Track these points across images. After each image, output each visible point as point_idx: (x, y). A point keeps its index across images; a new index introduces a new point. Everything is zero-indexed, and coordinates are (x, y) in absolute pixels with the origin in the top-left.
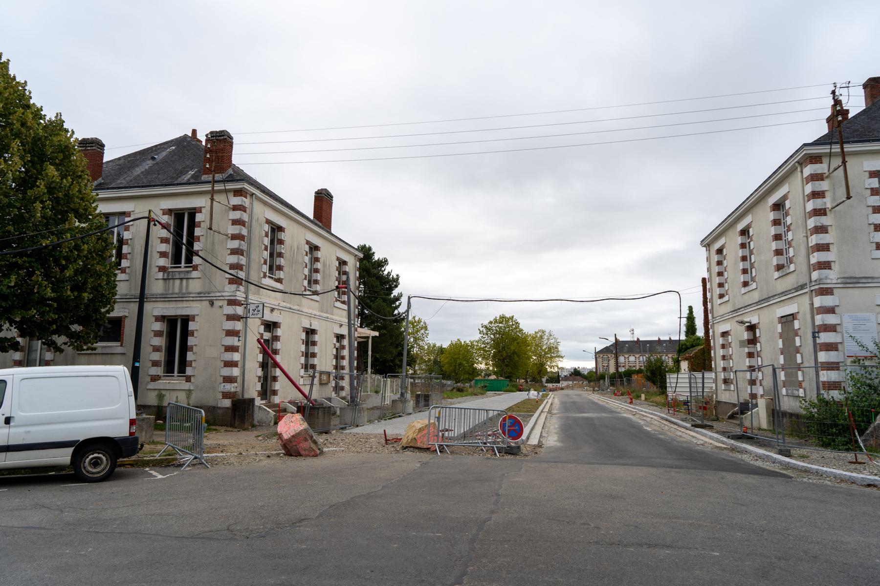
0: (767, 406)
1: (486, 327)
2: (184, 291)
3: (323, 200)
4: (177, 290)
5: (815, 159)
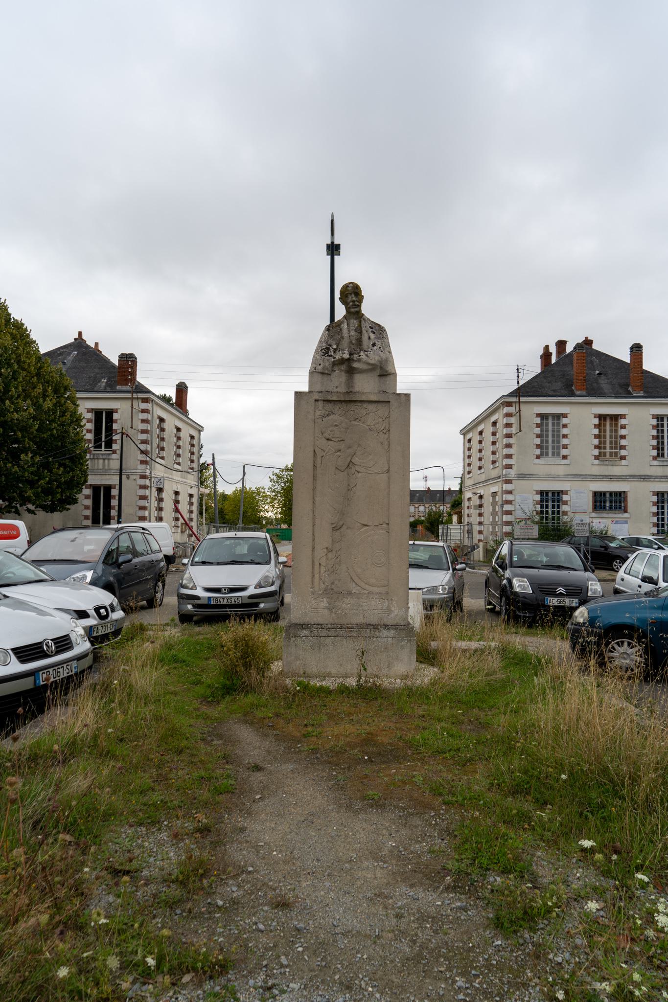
0: (483, 548)
1: (277, 475)
2: (106, 467)
3: (182, 390)
4: (101, 467)
5: (509, 404)
